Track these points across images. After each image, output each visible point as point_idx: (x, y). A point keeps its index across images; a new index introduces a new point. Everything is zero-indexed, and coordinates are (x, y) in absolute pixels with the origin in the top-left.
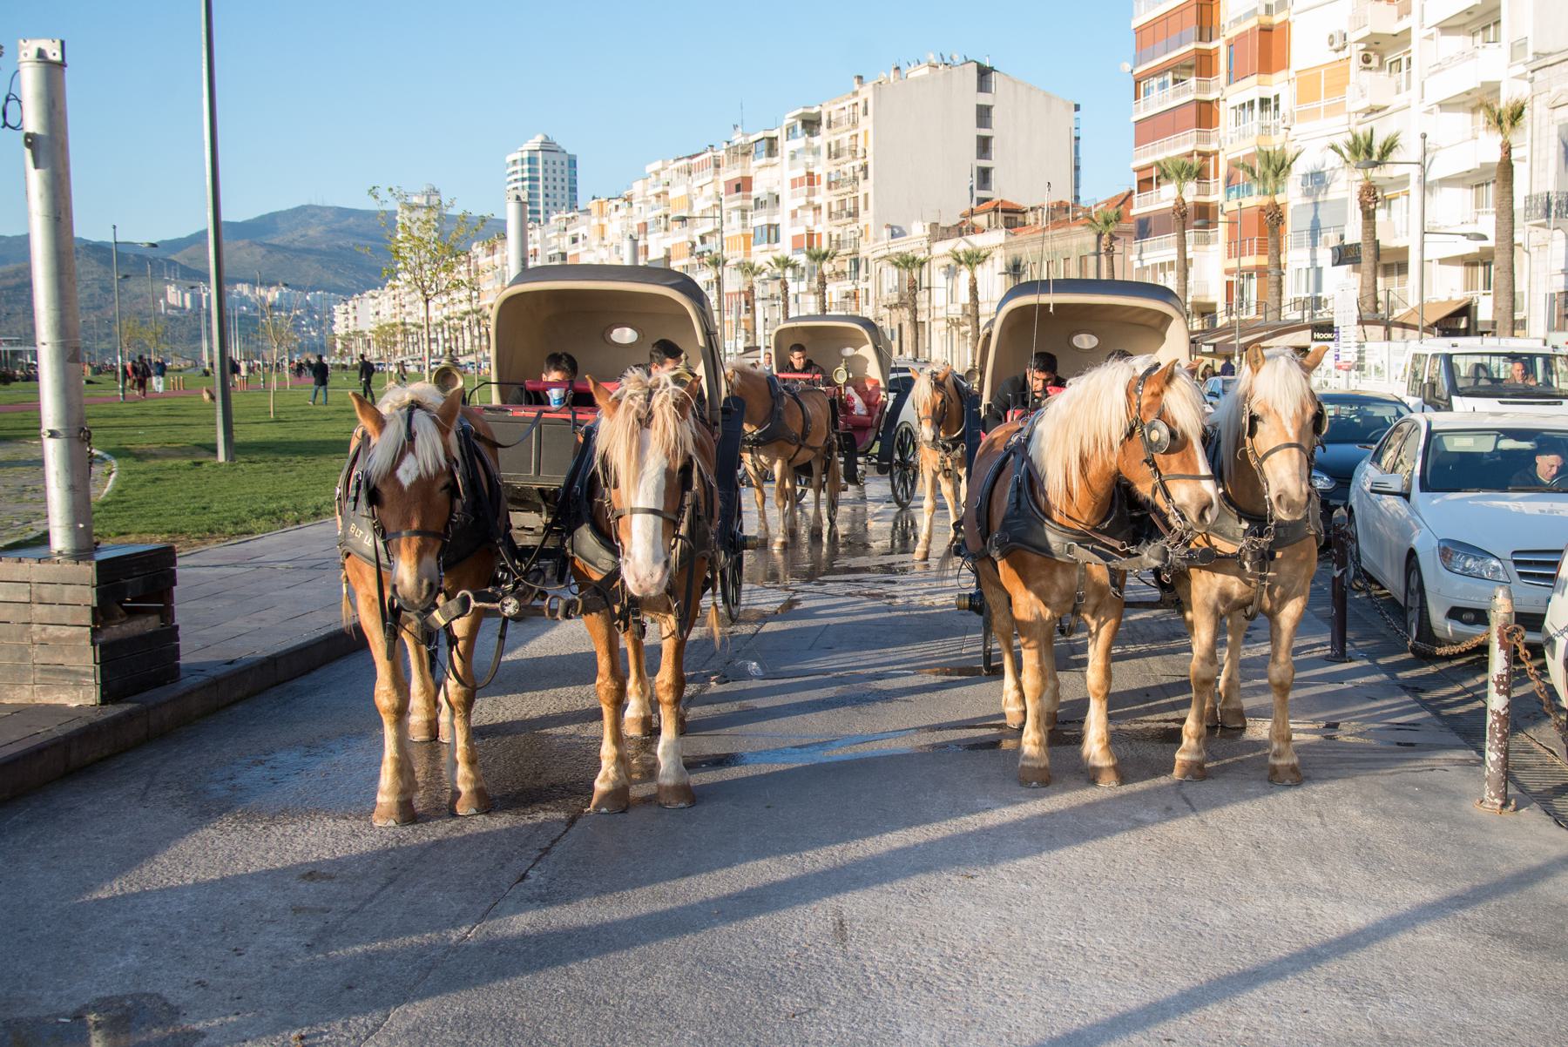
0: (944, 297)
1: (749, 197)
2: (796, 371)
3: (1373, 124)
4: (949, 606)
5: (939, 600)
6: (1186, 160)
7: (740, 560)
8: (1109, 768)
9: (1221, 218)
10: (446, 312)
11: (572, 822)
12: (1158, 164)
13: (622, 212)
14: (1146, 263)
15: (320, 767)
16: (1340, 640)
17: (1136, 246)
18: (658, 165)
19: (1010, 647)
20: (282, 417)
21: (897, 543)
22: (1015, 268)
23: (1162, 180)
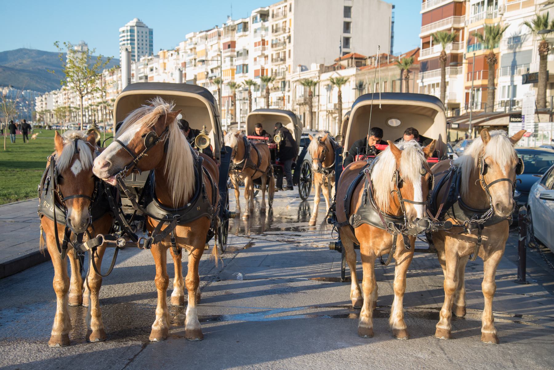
0: (325, 100)
1: (234, 51)
2: (258, 135)
3: (549, 10)
4: (326, 248)
5: (320, 245)
6: (447, 32)
7: (227, 223)
8: (403, 330)
9: (464, 61)
10: (90, 102)
11: (144, 346)
12: (433, 35)
13: (175, 56)
14: (425, 84)
15: (24, 318)
16: (522, 273)
17: (420, 75)
18: (191, 35)
19: (354, 269)
20: (10, 150)
21: (301, 217)
22: (360, 86)
23: (435, 42)
